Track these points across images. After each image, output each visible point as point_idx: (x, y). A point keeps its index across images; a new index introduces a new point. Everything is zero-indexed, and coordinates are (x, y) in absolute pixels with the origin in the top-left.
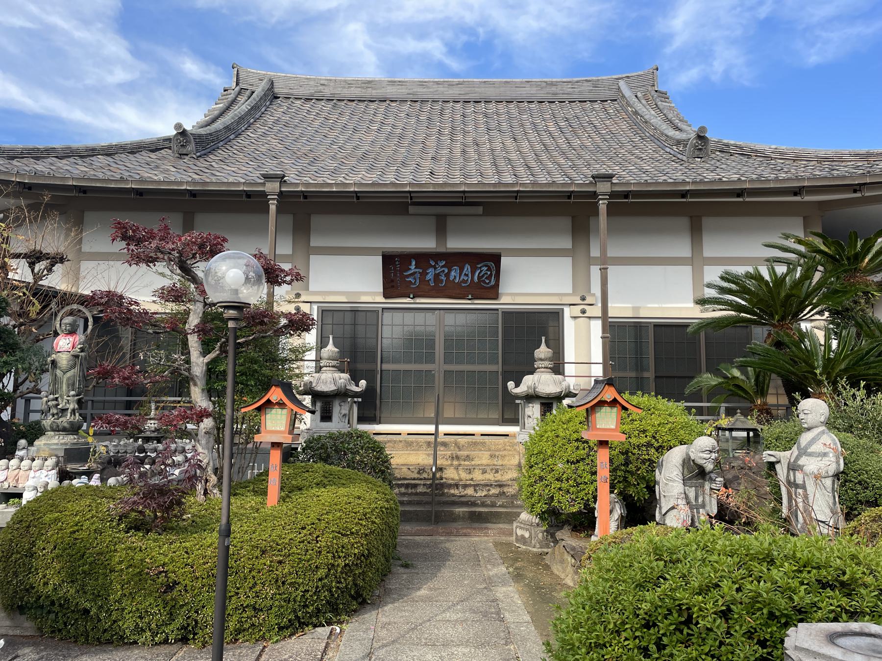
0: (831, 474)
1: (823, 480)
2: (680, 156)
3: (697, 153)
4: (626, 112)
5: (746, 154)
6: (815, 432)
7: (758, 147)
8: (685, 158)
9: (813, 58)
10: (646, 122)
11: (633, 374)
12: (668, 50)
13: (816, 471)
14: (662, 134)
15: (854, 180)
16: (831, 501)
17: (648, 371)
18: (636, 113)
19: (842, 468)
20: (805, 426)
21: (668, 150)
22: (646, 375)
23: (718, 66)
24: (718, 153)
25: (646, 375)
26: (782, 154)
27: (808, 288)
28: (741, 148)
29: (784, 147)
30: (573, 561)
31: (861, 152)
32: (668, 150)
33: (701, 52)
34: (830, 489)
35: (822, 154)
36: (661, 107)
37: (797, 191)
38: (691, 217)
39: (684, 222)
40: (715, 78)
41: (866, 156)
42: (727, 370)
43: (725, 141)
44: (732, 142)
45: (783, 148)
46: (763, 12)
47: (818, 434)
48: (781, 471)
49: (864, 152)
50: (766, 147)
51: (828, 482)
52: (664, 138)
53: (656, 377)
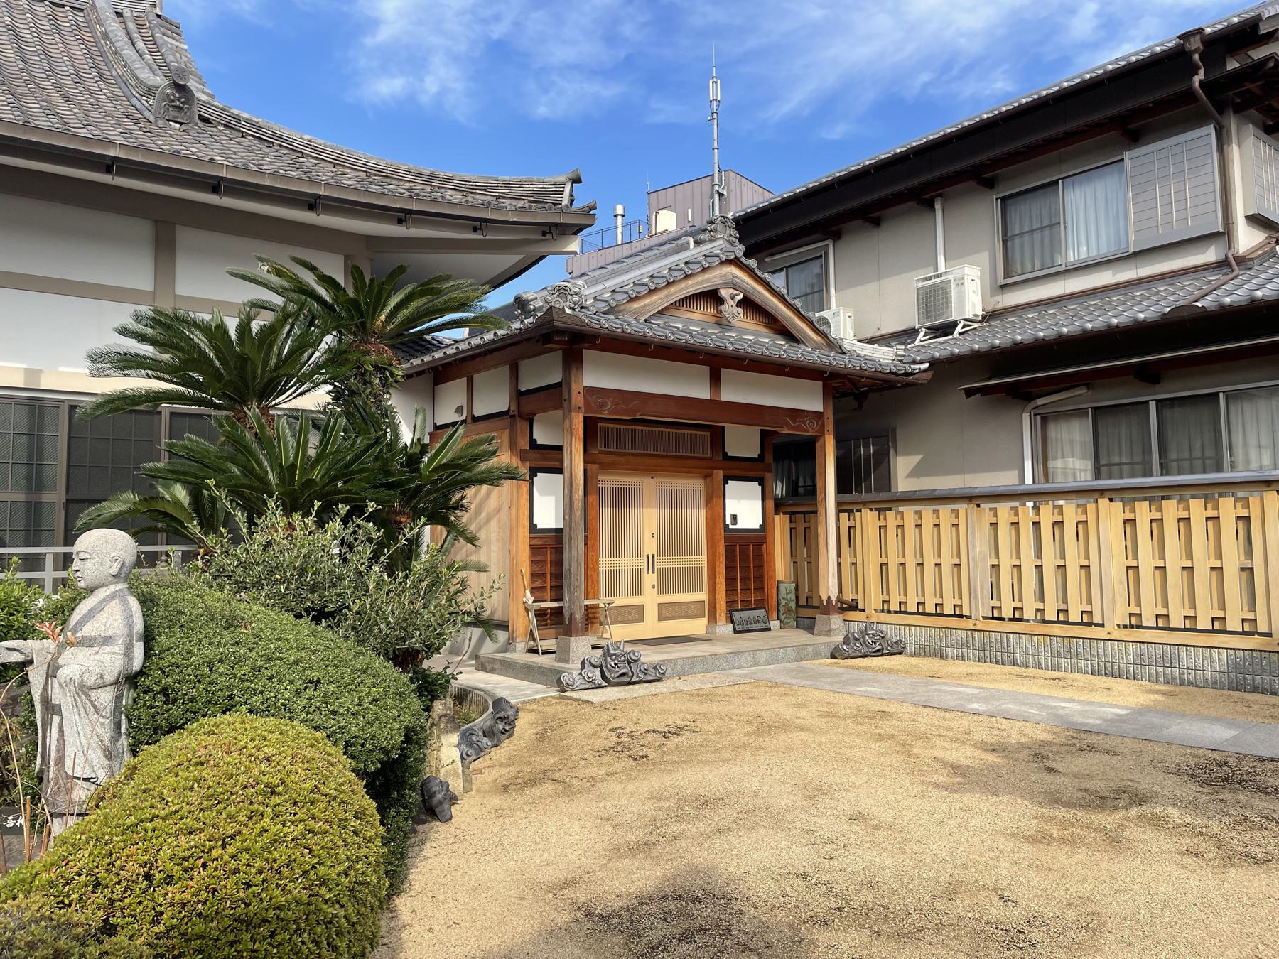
0: (109, 678)
1: (93, 694)
2: (147, 114)
3: (173, 113)
4: (93, 31)
5: (267, 140)
6: (101, 594)
7: (285, 132)
8: (152, 118)
9: (542, 111)
10: (116, 53)
11: (21, 496)
12: (369, 41)
13: (77, 677)
14: (133, 74)
15: (395, 202)
16: (107, 734)
17: (54, 488)
18: (106, 36)
19: (137, 663)
20: (81, 584)
21: (134, 101)
22: (47, 496)
23: (431, 85)
24: (221, 128)
25: (47, 496)
26: (317, 150)
27: (280, 353)
28: (259, 128)
29: (322, 142)
30: (354, 763)
31: (424, 172)
32: (134, 101)
33: (410, 58)
34: (107, 712)
35: (372, 162)
36: (159, 41)
37: (312, 203)
38: (156, 222)
39: (143, 228)
40: (424, 99)
41: (430, 179)
42: (167, 487)
43: (235, 111)
44: (246, 115)
45: (320, 142)
46: (498, 31)
47: (103, 600)
48: (36, 677)
49: (427, 172)
50: (299, 136)
51: (105, 698)
52: (133, 83)
53: (68, 501)
